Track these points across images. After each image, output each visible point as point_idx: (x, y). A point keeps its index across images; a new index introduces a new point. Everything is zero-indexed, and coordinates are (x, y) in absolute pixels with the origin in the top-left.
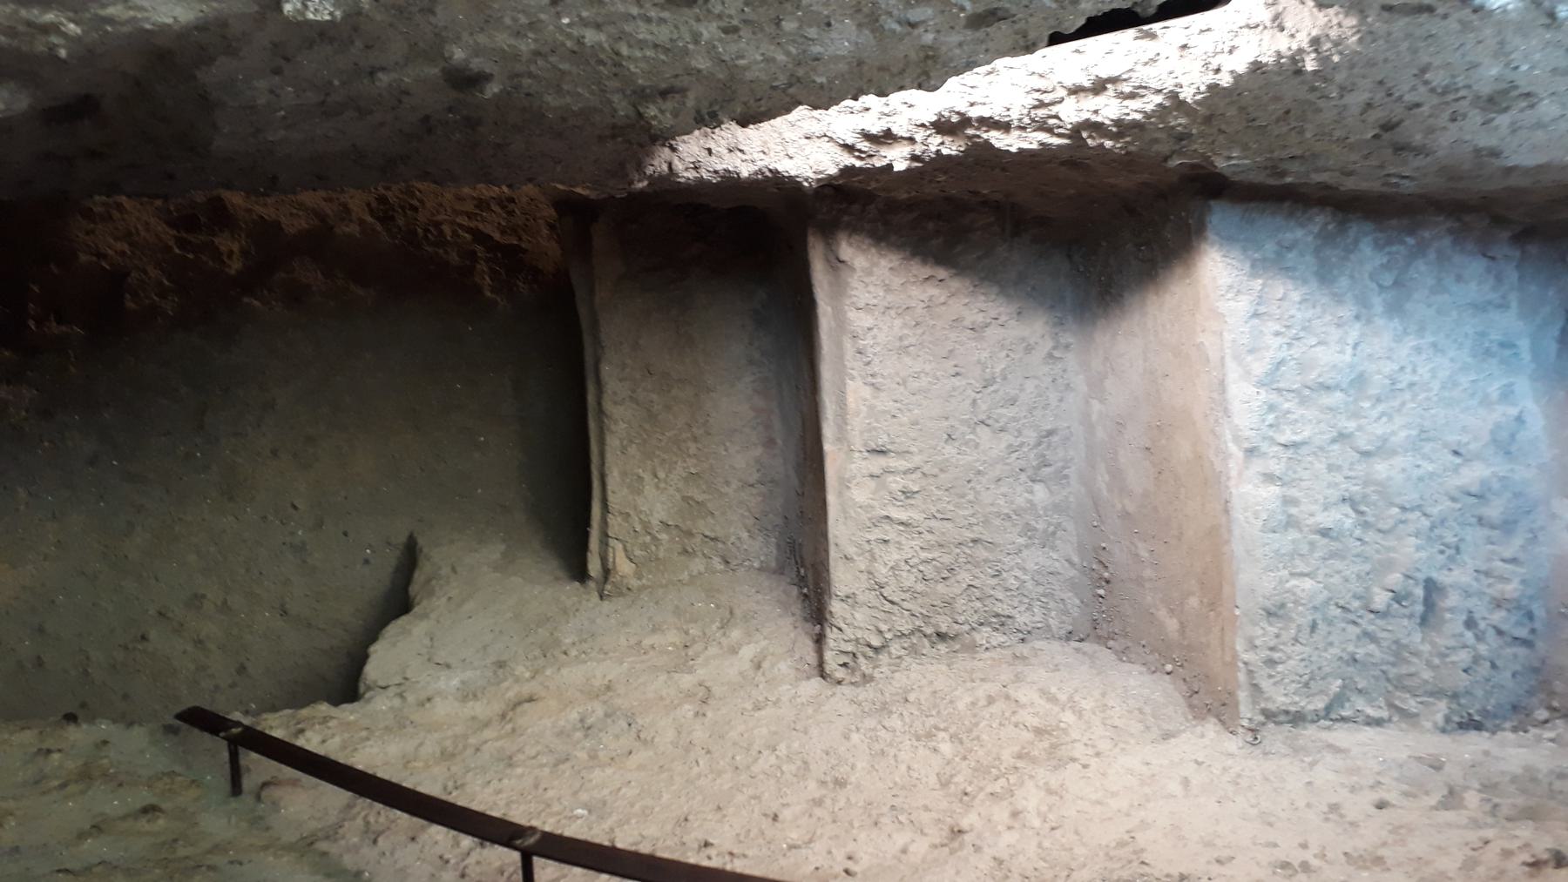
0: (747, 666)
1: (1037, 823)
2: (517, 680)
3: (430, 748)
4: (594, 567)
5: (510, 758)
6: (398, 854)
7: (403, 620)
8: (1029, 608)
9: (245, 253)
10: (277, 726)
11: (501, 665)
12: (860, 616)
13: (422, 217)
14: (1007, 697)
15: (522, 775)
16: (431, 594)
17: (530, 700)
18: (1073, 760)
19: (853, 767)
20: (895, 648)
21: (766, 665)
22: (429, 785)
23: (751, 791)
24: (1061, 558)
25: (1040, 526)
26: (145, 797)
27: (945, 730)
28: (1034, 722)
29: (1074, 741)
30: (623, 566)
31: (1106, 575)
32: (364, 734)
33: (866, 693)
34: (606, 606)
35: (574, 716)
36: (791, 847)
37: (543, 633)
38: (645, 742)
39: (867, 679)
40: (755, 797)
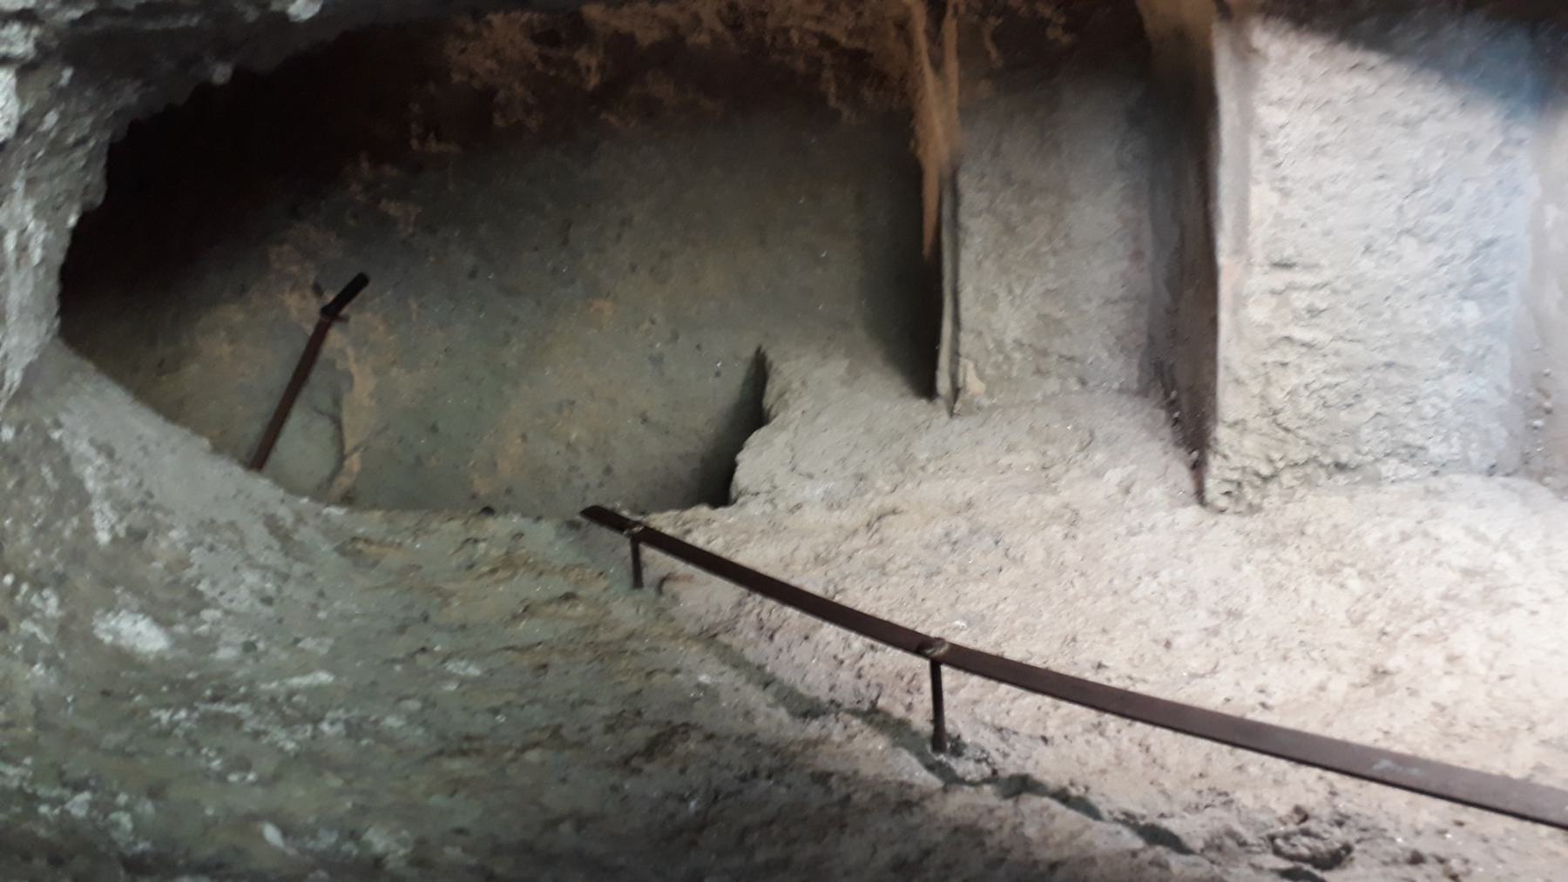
0: (1113, 490)
1: (1482, 670)
2: (878, 493)
3: (804, 553)
4: (943, 384)
5: (883, 567)
6: (794, 651)
7: (763, 431)
8: (1446, 439)
9: (602, 67)
10: (665, 522)
11: (861, 477)
12: (1249, 443)
13: (771, 23)
14: (1426, 534)
15: (898, 585)
16: (786, 405)
17: (894, 512)
18: (1517, 605)
19: (1248, 598)
20: (1287, 478)
21: (1135, 490)
22: (814, 584)
23: (1135, 616)
24: (1489, 387)
25: (1468, 348)
26: (560, 586)
27: (1352, 565)
28: (1464, 562)
29: (1515, 585)
30: (973, 384)
31: (1547, 404)
32: (743, 536)
33: (1254, 524)
34: (957, 424)
35: (939, 531)
36: (1193, 676)
37: (898, 448)
38: (1014, 560)
39: (1253, 509)
40: (1139, 622)
